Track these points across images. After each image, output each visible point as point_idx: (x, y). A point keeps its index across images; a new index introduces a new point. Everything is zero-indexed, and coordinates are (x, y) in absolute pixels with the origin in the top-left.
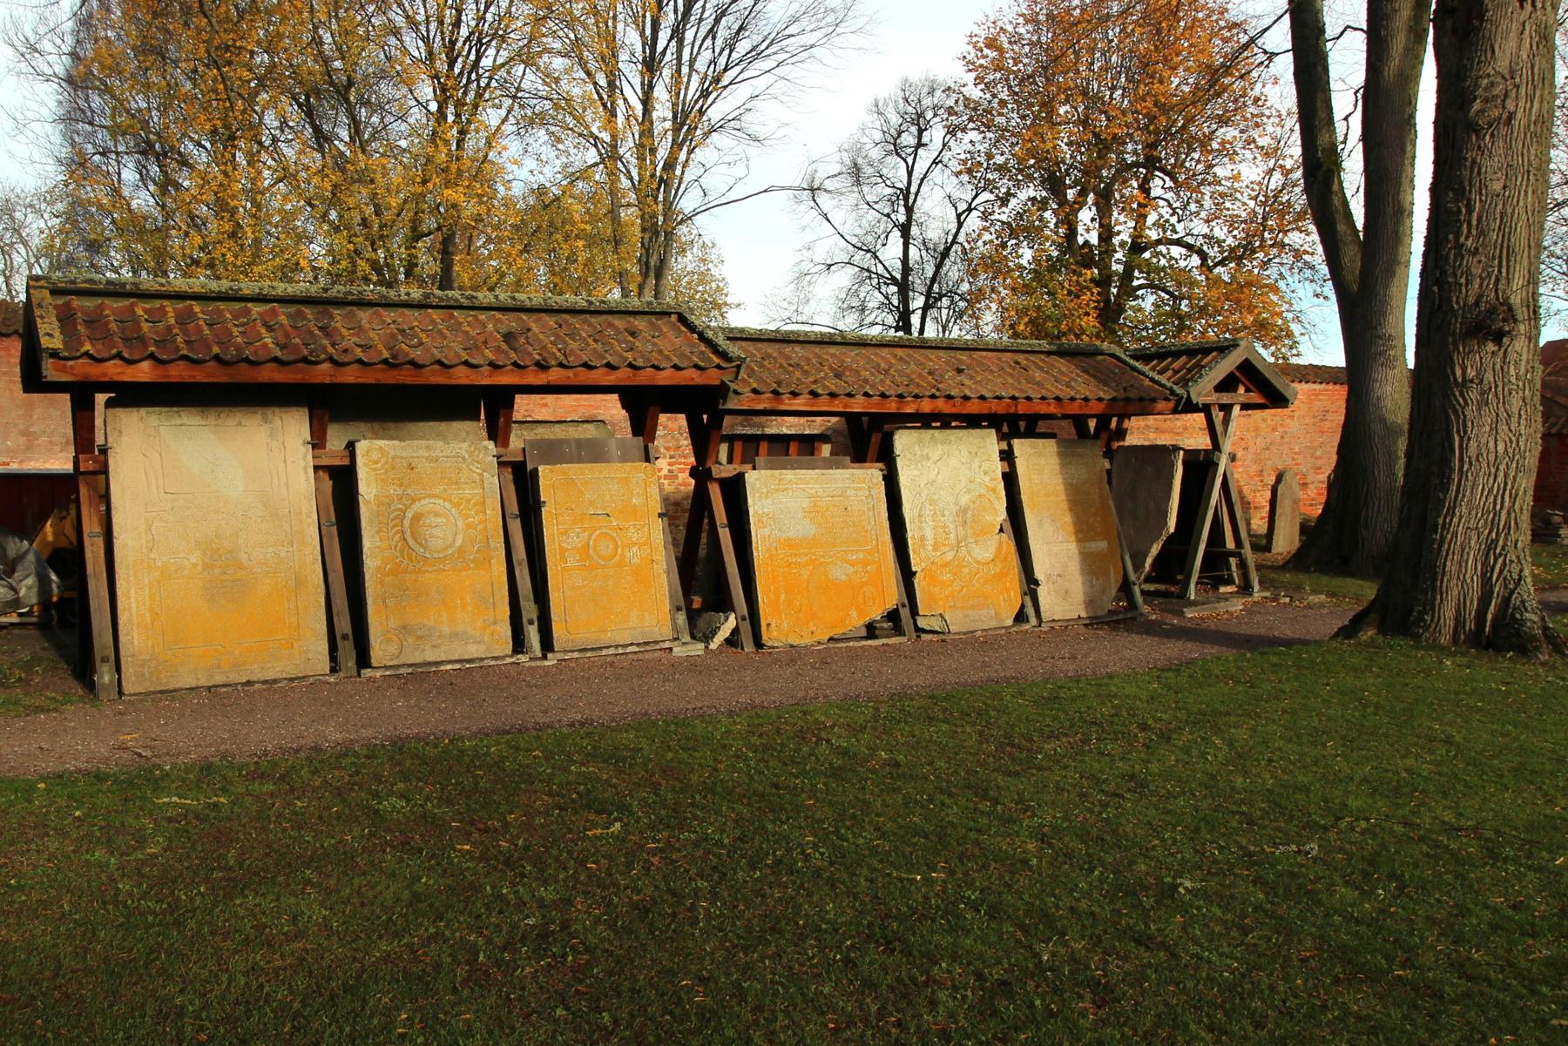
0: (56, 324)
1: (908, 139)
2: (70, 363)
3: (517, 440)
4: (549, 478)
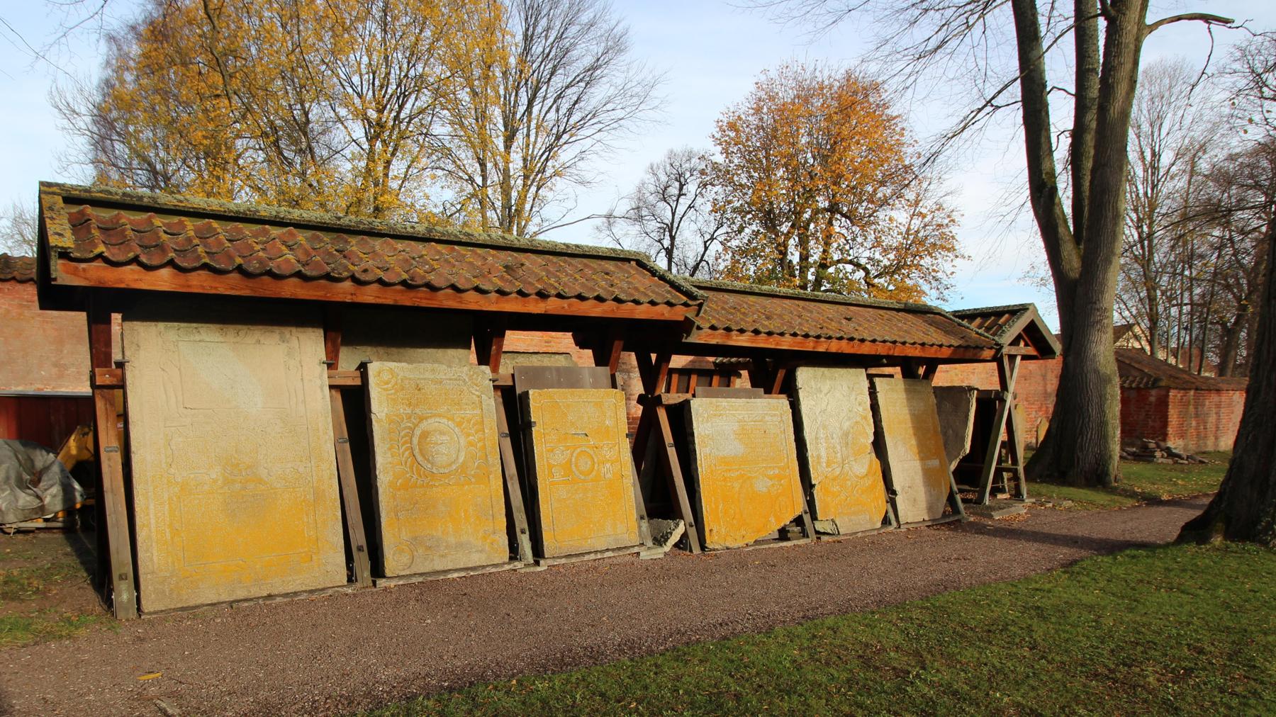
0: (67, 226)
1: (674, 190)
2: (83, 265)
3: (507, 367)
4: (540, 403)
